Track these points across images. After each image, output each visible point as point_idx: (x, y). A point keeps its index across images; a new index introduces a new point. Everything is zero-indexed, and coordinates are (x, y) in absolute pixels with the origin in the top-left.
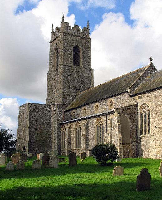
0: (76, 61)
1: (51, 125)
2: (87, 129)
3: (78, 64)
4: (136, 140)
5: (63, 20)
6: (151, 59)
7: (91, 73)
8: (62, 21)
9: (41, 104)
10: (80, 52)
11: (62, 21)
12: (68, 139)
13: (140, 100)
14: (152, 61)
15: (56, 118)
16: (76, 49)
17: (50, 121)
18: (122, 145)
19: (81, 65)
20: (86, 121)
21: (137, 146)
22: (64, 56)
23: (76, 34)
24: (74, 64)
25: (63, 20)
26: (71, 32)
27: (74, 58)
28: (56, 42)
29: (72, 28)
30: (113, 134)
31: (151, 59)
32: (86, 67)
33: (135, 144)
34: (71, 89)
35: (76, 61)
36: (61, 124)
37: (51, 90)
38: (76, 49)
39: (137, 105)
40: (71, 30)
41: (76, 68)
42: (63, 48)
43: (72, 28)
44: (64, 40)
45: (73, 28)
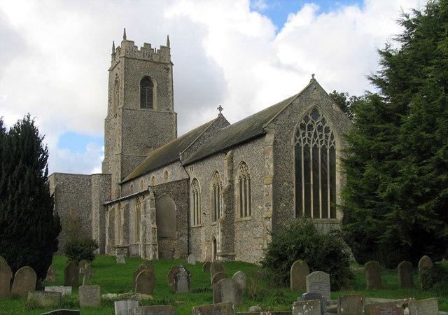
0: (146, 100)
1: (91, 206)
2: (127, 215)
3: (151, 106)
4: (187, 232)
5: (125, 37)
6: (220, 109)
7: (172, 119)
8: (123, 40)
9: (76, 175)
10: (153, 86)
11: (123, 40)
12: (109, 228)
13: (193, 173)
14: (222, 112)
15: (97, 196)
16: (146, 82)
17: (90, 200)
18: (156, 240)
19: (155, 107)
20: (126, 202)
21: (188, 241)
22: (125, 94)
23: (146, 58)
24: (143, 106)
25: (125, 37)
26: (138, 56)
27: (143, 96)
28: (116, 70)
29: (139, 49)
30: (240, 214)
31: (220, 109)
32: (164, 110)
33: (185, 239)
34: (136, 147)
35: (146, 100)
36: (105, 205)
37: (110, 147)
38: (146, 82)
39: (189, 179)
40: (138, 51)
41: (146, 112)
42: (123, 81)
43: (139, 49)
44: (125, 68)
45: (142, 48)
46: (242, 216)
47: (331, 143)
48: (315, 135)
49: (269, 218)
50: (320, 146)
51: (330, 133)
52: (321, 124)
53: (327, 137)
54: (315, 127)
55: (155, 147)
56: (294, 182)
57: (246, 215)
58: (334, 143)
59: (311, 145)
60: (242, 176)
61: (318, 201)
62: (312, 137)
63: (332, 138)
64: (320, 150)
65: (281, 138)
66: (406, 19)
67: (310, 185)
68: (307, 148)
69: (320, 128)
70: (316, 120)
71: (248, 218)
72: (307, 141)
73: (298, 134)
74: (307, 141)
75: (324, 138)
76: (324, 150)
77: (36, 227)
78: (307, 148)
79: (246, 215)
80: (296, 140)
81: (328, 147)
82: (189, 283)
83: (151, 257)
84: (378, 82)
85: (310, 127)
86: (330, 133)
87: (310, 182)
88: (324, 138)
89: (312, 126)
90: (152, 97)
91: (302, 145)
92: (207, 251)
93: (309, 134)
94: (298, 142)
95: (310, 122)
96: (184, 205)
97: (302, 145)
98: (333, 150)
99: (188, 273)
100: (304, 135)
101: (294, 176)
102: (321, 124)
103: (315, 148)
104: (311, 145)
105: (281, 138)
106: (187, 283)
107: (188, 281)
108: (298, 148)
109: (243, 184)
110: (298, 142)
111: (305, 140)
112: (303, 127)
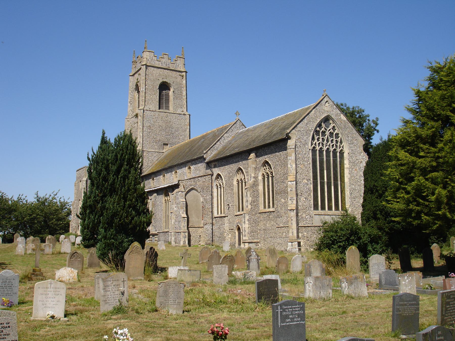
3: (167, 108)
41: (162, 114)
46: (265, 207)
47: (340, 147)
48: (328, 141)
49: (293, 210)
50: (332, 149)
51: (339, 138)
52: (332, 131)
53: (337, 142)
54: (327, 133)
55: (172, 144)
56: (312, 179)
57: (269, 207)
58: (343, 147)
59: (325, 148)
60: (265, 174)
61: (317, 194)
62: (325, 141)
63: (341, 142)
64: (318, 152)
65: (300, 142)
66: (430, 65)
67: (324, 182)
68: (321, 151)
69: (331, 134)
70: (328, 127)
71: (271, 209)
72: (321, 144)
73: (313, 139)
74: (321, 144)
75: (321, 140)
76: (335, 152)
77: (139, 217)
78: (321, 151)
79: (269, 207)
80: (312, 144)
81: (338, 150)
82: (258, 265)
83: (182, 243)
84: (411, 110)
85: (324, 133)
86: (339, 138)
87: (324, 180)
88: (334, 142)
89: (325, 132)
90: (169, 100)
91: (318, 148)
92: (231, 238)
93: (323, 139)
94: (314, 145)
95: (323, 129)
96: (209, 197)
97: (318, 148)
98: (342, 153)
99: (258, 256)
100: (318, 139)
101: (311, 174)
102: (332, 131)
103: (328, 151)
104: (325, 148)
105: (300, 142)
106: (257, 264)
107: (258, 263)
108: (314, 150)
109: (266, 179)
110: (314, 145)
111: (319, 144)
112: (317, 132)
